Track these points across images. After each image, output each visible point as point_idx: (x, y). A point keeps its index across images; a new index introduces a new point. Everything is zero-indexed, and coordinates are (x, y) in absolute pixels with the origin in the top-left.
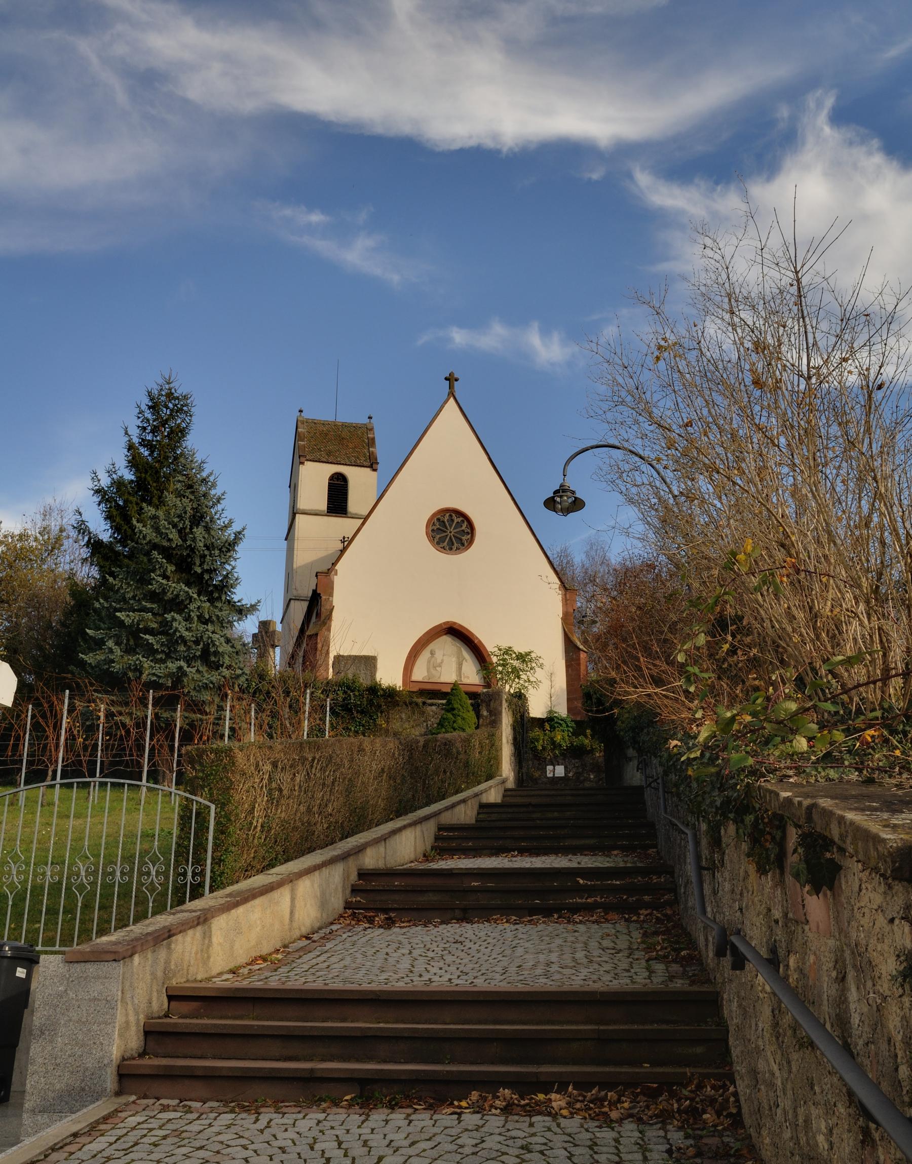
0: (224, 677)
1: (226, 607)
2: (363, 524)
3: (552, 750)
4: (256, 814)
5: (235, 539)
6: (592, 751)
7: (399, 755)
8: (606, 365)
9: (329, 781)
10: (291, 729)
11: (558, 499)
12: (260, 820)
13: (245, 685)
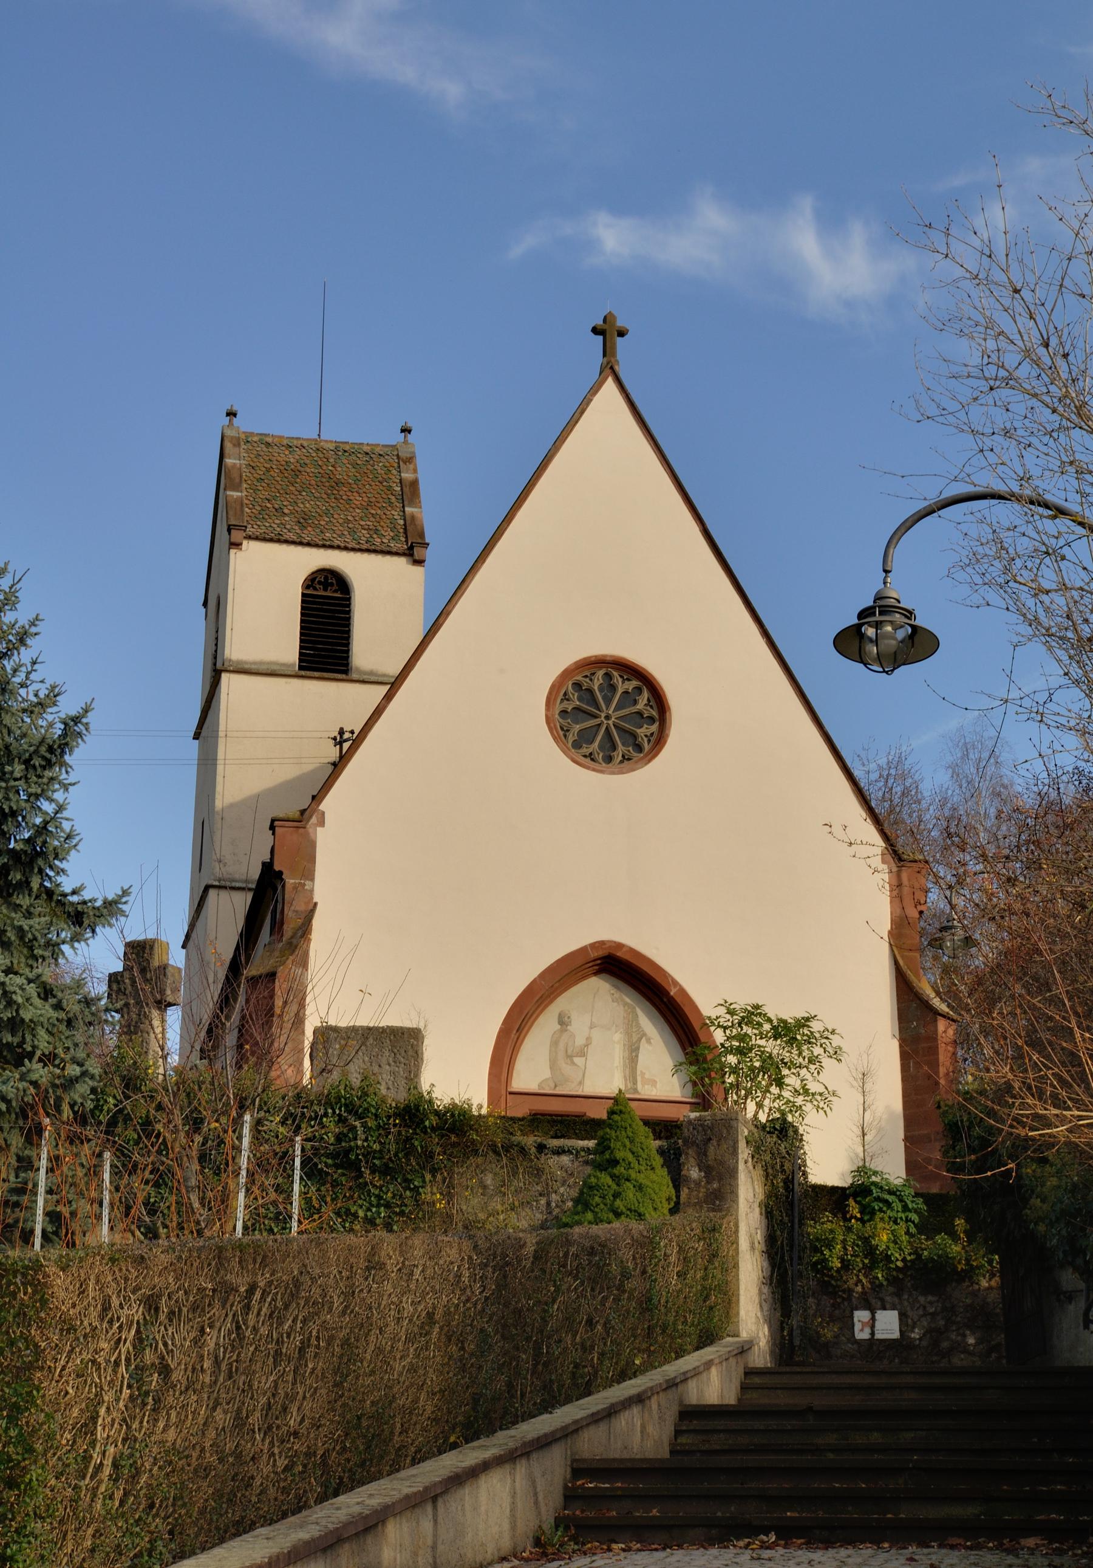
0: (35, 1084)
1: (41, 906)
2: (389, 697)
3: (869, 1269)
4: (100, 1434)
5: (64, 735)
6: (969, 1274)
7: (473, 1277)
8: (968, 285)
9: (290, 1347)
10: (202, 1214)
11: (871, 632)
12: (111, 1450)
13: (90, 1105)
